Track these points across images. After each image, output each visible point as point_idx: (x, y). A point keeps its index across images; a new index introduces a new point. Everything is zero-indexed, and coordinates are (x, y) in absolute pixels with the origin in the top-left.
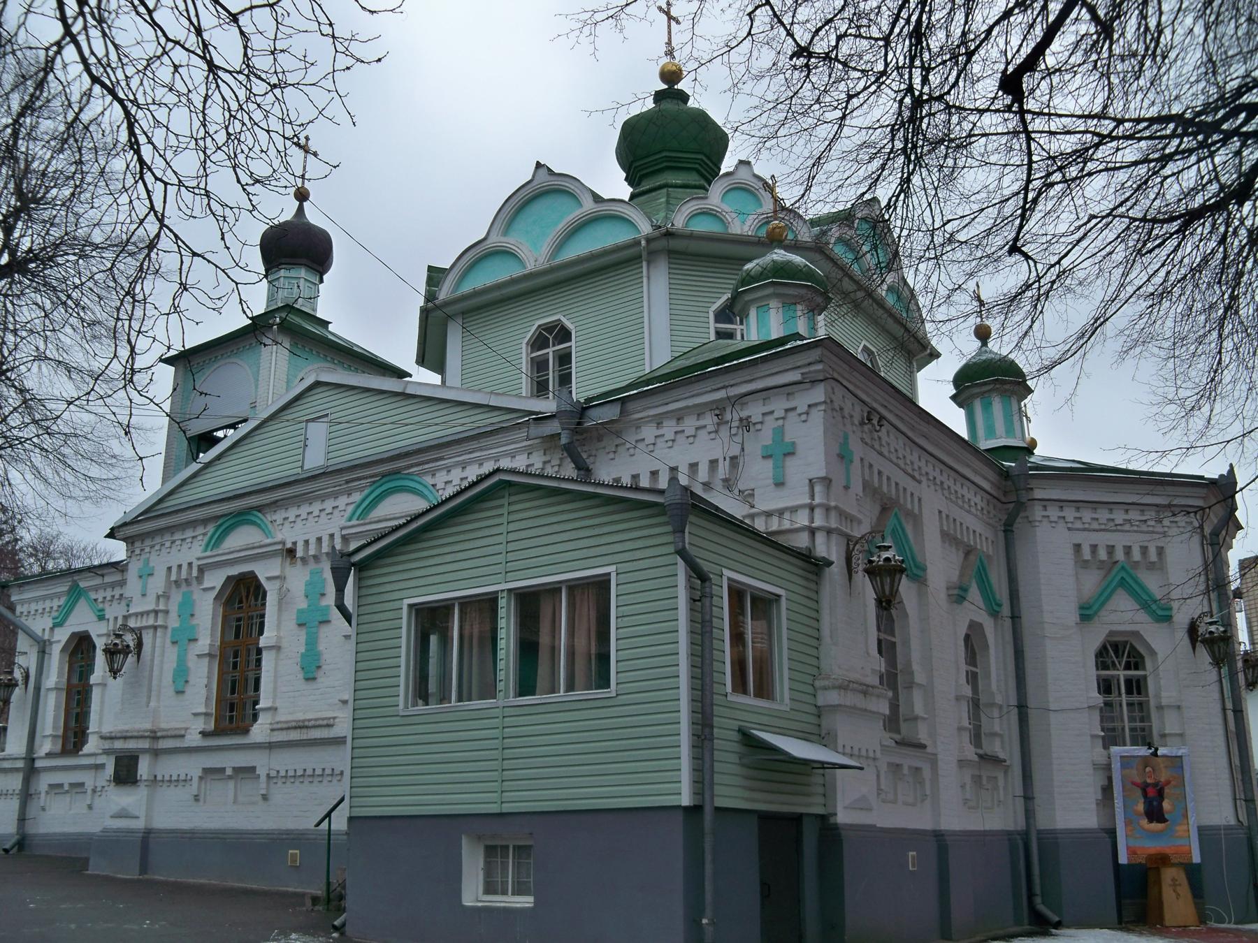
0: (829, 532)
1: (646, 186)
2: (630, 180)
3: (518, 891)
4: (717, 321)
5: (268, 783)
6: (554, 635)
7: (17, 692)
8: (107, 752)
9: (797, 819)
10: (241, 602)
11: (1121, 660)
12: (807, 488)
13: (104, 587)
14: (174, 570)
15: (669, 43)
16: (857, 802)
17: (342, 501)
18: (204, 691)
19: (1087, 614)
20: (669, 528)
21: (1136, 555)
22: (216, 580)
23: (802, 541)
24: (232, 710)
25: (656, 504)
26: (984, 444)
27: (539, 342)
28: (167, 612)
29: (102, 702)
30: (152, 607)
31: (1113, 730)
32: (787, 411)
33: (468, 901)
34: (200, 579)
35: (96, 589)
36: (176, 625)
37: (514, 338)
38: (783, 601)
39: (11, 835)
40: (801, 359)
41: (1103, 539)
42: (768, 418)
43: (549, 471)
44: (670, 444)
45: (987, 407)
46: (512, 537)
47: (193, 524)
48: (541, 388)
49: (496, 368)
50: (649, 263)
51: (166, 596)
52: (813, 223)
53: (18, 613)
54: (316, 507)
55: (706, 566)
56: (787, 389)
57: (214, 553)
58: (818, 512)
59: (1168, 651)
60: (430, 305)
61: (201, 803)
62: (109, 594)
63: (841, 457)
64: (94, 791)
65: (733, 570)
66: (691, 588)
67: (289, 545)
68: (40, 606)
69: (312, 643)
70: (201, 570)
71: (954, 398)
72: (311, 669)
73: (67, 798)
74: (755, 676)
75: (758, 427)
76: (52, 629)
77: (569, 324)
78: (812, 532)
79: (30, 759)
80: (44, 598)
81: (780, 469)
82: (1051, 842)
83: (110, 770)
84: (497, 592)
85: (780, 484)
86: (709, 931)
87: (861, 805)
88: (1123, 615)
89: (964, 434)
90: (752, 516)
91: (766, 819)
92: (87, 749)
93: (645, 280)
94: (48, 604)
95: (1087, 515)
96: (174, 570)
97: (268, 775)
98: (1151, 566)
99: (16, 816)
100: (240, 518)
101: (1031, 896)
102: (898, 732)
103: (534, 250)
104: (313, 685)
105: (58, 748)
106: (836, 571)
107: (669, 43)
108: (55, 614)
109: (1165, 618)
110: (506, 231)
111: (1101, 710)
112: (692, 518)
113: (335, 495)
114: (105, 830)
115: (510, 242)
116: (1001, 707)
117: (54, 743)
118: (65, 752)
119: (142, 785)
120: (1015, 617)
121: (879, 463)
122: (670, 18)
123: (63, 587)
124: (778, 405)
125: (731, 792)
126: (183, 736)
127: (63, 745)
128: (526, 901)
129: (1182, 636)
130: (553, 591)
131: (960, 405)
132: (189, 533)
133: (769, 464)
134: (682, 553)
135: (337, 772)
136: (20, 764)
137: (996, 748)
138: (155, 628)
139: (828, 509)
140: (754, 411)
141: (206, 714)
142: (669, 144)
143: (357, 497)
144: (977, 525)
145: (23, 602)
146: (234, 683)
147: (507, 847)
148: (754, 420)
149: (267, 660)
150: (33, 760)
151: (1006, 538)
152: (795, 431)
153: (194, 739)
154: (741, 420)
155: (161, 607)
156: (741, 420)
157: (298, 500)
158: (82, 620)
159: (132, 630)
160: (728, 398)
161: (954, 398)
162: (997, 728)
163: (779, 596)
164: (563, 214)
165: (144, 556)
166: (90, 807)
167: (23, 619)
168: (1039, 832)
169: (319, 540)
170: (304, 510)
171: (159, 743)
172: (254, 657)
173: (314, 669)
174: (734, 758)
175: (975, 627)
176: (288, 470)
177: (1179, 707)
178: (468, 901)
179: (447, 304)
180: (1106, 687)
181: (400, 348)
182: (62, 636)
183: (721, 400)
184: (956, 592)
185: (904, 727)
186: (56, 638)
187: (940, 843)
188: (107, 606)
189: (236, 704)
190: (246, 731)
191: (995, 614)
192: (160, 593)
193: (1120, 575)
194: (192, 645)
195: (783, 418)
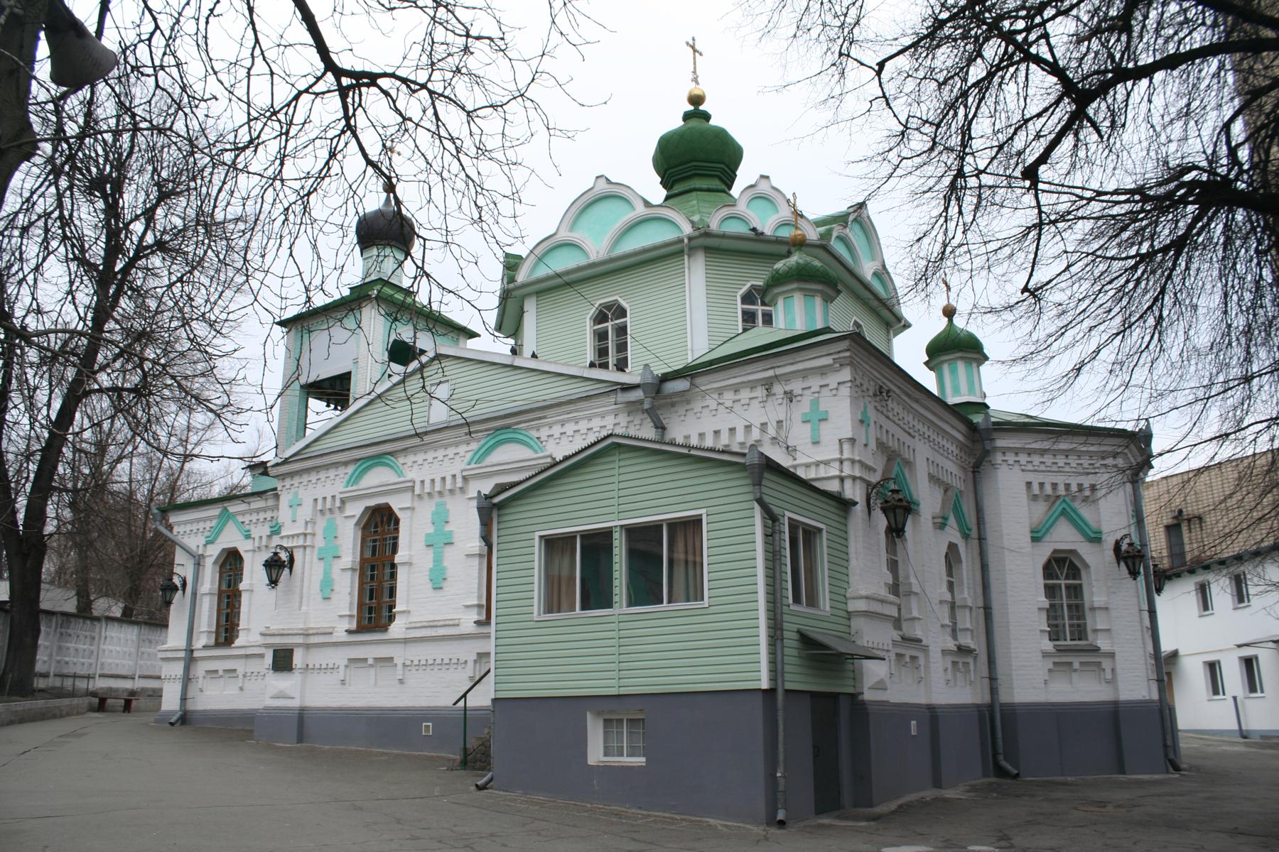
0: (854, 478)
1: (678, 188)
2: (664, 184)
4: (743, 303)
6: (657, 561)
8: (267, 646)
9: (835, 696)
10: (376, 526)
11: (1062, 569)
12: (837, 447)
13: (251, 512)
14: (320, 501)
15: (694, 72)
16: (881, 682)
17: (462, 449)
18: (348, 598)
19: (1036, 539)
20: (749, 481)
22: (356, 510)
23: (833, 487)
24: (370, 613)
25: (736, 463)
26: (951, 400)
27: (601, 317)
28: (314, 535)
29: (250, 604)
31: (1056, 626)
33: (592, 761)
35: (243, 513)
38: (824, 534)
39: (176, 712)
40: (833, 348)
41: (1048, 480)
42: (806, 392)
43: (632, 432)
45: (953, 372)
46: (622, 485)
47: (336, 465)
50: (689, 256)
51: (313, 522)
52: (818, 223)
55: (776, 510)
56: (822, 371)
57: (355, 488)
59: (1098, 561)
60: (511, 286)
62: (254, 517)
63: (862, 422)
64: (244, 676)
65: (792, 511)
66: (765, 526)
68: (194, 527)
69: (438, 560)
70: (343, 501)
71: (926, 363)
72: (438, 581)
74: (805, 592)
76: (205, 545)
78: (842, 479)
80: (198, 520)
81: (815, 431)
82: (1012, 714)
83: (269, 659)
85: (816, 443)
86: (782, 782)
87: (881, 686)
88: (1064, 537)
89: (935, 392)
90: (795, 467)
91: (813, 695)
92: (237, 643)
94: (201, 525)
95: (1036, 459)
96: (320, 501)
98: (1086, 499)
99: (179, 696)
100: (378, 460)
101: (995, 755)
102: (900, 629)
103: (597, 243)
104: (439, 593)
105: (212, 642)
106: (860, 509)
107: (694, 72)
108: (207, 534)
109: (1096, 539)
110: (571, 229)
111: (1048, 610)
112: (766, 475)
113: (457, 445)
114: (266, 708)
115: (576, 236)
116: (971, 608)
117: (209, 638)
118: (218, 645)
119: (296, 673)
120: (981, 539)
121: (887, 425)
122: (695, 51)
123: (215, 511)
124: (815, 382)
125: (796, 679)
127: (359, 622)
128: (640, 760)
129: (1110, 554)
131: (931, 369)
132: (332, 473)
133: (808, 426)
134: (760, 501)
136: (182, 654)
137: (966, 640)
138: (305, 547)
140: (796, 386)
141: (351, 616)
142: (698, 158)
144: (952, 469)
145: (179, 524)
146: (372, 591)
147: (622, 720)
148: (795, 393)
151: (974, 478)
152: (827, 402)
153: (341, 629)
154: (785, 393)
155: (309, 531)
156: (785, 393)
158: (231, 538)
159: (286, 549)
161: (926, 363)
162: (915, 614)
163: (820, 530)
164: (618, 216)
165: (293, 490)
166: (241, 689)
168: (1002, 705)
169: (444, 479)
171: (316, 640)
172: (388, 571)
173: (442, 575)
174: (795, 652)
175: (952, 547)
177: (1107, 609)
178: (592, 761)
179: (524, 286)
180: (1051, 591)
182: (214, 552)
184: (940, 520)
185: (905, 625)
187: (932, 715)
189: (375, 607)
190: (384, 628)
191: (966, 537)
193: (1062, 505)
194: (336, 561)
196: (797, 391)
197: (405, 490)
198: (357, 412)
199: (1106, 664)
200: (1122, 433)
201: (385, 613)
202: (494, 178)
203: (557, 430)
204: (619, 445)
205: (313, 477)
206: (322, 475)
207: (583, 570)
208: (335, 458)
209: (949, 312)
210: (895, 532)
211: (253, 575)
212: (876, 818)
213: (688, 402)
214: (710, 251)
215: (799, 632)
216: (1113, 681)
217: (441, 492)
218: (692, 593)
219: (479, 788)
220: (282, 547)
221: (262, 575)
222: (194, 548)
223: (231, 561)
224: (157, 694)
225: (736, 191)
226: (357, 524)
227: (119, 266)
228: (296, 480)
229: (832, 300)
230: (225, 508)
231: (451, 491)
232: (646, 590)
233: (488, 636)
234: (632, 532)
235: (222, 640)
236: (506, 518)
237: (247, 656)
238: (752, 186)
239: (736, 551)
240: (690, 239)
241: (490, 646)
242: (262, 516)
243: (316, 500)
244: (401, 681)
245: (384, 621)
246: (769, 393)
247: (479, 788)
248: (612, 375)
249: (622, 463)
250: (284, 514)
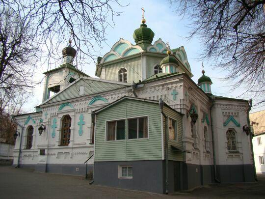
0: (184, 109)
1: (139, 42)
3: (129, 176)
6: (137, 128)
7: (18, 137)
11: (231, 132)
13: (36, 117)
16: (191, 159)
17: (87, 101)
19: (225, 125)
21: (234, 114)
22: (61, 116)
23: (179, 111)
27: (120, 72)
34: (57, 115)
35: (34, 117)
37: (115, 70)
41: (228, 111)
47: (57, 105)
48: (121, 80)
49: (111, 75)
51: (50, 119)
52: (173, 50)
54: (82, 102)
56: (176, 82)
58: (182, 105)
59: (239, 130)
69: (81, 128)
70: (58, 114)
72: (81, 133)
77: (126, 69)
78: (181, 109)
79: (20, 150)
80: (23, 119)
82: (219, 167)
87: (190, 160)
88: (231, 125)
92: (32, 148)
95: (225, 106)
100: (66, 104)
109: (239, 126)
114: (38, 164)
118: (27, 148)
120: (212, 126)
123: (27, 117)
125: (171, 158)
128: (132, 177)
132: (55, 107)
133: (173, 96)
134: (162, 113)
136: (19, 151)
137: (208, 149)
139: (184, 105)
140: (170, 86)
142: (145, 35)
143: (90, 101)
144: (205, 108)
147: (126, 168)
149: (72, 132)
153: (57, 146)
157: (78, 101)
158: (31, 123)
170: (79, 103)
173: (81, 134)
175: (205, 127)
176: (77, 95)
180: (228, 138)
181: (197, 83)
182: (27, 126)
189: (65, 139)
190: (67, 145)
191: (208, 125)
193: (231, 118)
197: (73, 111)
198: (62, 92)
199: (241, 156)
200: (245, 101)
201: (67, 141)
202: (98, 26)
203: (110, 97)
205: (51, 108)
206: (53, 108)
207: (118, 130)
208: (54, 104)
209: (203, 72)
210: (194, 122)
211: (36, 131)
212: (189, 192)
213: (143, 90)
214: (147, 56)
215: (171, 146)
216: (242, 160)
219: (90, 184)
221: (38, 132)
223: (31, 129)
224: (12, 161)
225: (153, 43)
227: (6, 58)
229: (177, 67)
232: (132, 136)
233: (93, 147)
234: (130, 121)
237: (34, 151)
239: (156, 124)
241: (93, 149)
242: (38, 118)
245: (67, 143)
247: (90, 184)
248: (123, 83)
250: (43, 117)
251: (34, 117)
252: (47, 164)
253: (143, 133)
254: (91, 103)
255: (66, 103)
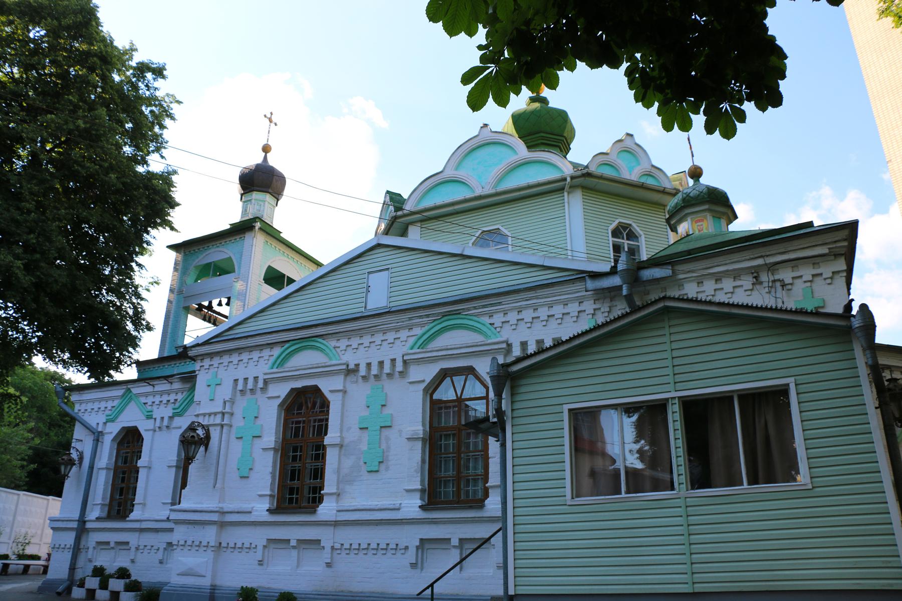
5: (332, 553)
13: (154, 394)
17: (403, 334)
22: (281, 391)
28: (232, 414)
29: (148, 477)
30: (220, 409)
32: (813, 276)
34: (264, 389)
35: (146, 395)
36: (241, 424)
39: (61, 581)
42: (796, 281)
44: (829, 281)
47: (260, 347)
50: (569, 193)
51: (232, 401)
53: (76, 411)
54: (378, 338)
56: (814, 260)
60: (399, 213)
61: (265, 566)
62: (157, 399)
64: (137, 549)
67: (352, 366)
68: (96, 406)
70: (266, 382)
73: (112, 552)
75: (789, 287)
76: (105, 423)
79: (82, 521)
80: (100, 400)
84: (667, 400)
92: (132, 516)
93: (566, 204)
94: (103, 405)
97: (333, 548)
105: (104, 514)
108: (108, 412)
110: (456, 169)
113: (397, 330)
115: (461, 174)
118: (110, 517)
124: (807, 272)
126: (250, 512)
127: (109, 512)
130: (725, 400)
132: (255, 355)
135: (401, 546)
136: (75, 525)
138: (222, 426)
140: (786, 275)
145: (81, 402)
149: (331, 456)
150: (85, 522)
153: (261, 508)
155: (227, 409)
157: (349, 334)
158: (131, 417)
159: (203, 427)
160: (766, 264)
165: (212, 370)
166: (329, 565)
167: (80, 414)
170: (366, 340)
176: (355, 309)
182: (113, 429)
183: (759, 266)
186: (108, 430)
188: (155, 407)
189: (300, 481)
190: (314, 512)
192: (227, 399)
194: (257, 441)
195: (810, 281)
196: (788, 280)
203: (513, 317)
204: (667, 309)
205: (235, 358)
206: (245, 356)
214: (584, 188)
217: (379, 374)
218: (761, 474)
220: (200, 425)
222: (94, 426)
226: (281, 405)
228: (216, 361)
230: (129, 389)
231: (390, 375)
235: (114, 512)
236: (523, 389)
237: (142, 530)
238: (620, 141)
240: (572, 178)
242: (165, 398)
243: (236, 381)
244: (329, 565)
246: (757, 281)
249: (673, 330)
251: (146, 395)
252: (214, 588)
253: (771, 462)
254: (282, 361)
255: (307, 335)
